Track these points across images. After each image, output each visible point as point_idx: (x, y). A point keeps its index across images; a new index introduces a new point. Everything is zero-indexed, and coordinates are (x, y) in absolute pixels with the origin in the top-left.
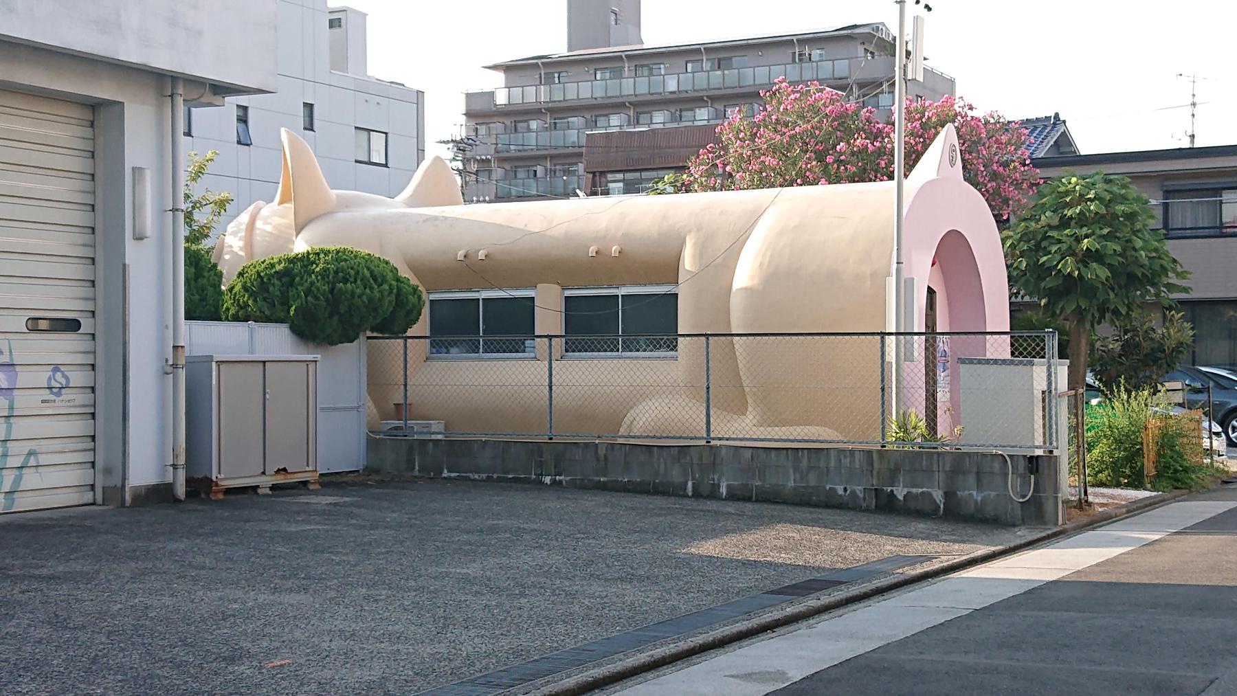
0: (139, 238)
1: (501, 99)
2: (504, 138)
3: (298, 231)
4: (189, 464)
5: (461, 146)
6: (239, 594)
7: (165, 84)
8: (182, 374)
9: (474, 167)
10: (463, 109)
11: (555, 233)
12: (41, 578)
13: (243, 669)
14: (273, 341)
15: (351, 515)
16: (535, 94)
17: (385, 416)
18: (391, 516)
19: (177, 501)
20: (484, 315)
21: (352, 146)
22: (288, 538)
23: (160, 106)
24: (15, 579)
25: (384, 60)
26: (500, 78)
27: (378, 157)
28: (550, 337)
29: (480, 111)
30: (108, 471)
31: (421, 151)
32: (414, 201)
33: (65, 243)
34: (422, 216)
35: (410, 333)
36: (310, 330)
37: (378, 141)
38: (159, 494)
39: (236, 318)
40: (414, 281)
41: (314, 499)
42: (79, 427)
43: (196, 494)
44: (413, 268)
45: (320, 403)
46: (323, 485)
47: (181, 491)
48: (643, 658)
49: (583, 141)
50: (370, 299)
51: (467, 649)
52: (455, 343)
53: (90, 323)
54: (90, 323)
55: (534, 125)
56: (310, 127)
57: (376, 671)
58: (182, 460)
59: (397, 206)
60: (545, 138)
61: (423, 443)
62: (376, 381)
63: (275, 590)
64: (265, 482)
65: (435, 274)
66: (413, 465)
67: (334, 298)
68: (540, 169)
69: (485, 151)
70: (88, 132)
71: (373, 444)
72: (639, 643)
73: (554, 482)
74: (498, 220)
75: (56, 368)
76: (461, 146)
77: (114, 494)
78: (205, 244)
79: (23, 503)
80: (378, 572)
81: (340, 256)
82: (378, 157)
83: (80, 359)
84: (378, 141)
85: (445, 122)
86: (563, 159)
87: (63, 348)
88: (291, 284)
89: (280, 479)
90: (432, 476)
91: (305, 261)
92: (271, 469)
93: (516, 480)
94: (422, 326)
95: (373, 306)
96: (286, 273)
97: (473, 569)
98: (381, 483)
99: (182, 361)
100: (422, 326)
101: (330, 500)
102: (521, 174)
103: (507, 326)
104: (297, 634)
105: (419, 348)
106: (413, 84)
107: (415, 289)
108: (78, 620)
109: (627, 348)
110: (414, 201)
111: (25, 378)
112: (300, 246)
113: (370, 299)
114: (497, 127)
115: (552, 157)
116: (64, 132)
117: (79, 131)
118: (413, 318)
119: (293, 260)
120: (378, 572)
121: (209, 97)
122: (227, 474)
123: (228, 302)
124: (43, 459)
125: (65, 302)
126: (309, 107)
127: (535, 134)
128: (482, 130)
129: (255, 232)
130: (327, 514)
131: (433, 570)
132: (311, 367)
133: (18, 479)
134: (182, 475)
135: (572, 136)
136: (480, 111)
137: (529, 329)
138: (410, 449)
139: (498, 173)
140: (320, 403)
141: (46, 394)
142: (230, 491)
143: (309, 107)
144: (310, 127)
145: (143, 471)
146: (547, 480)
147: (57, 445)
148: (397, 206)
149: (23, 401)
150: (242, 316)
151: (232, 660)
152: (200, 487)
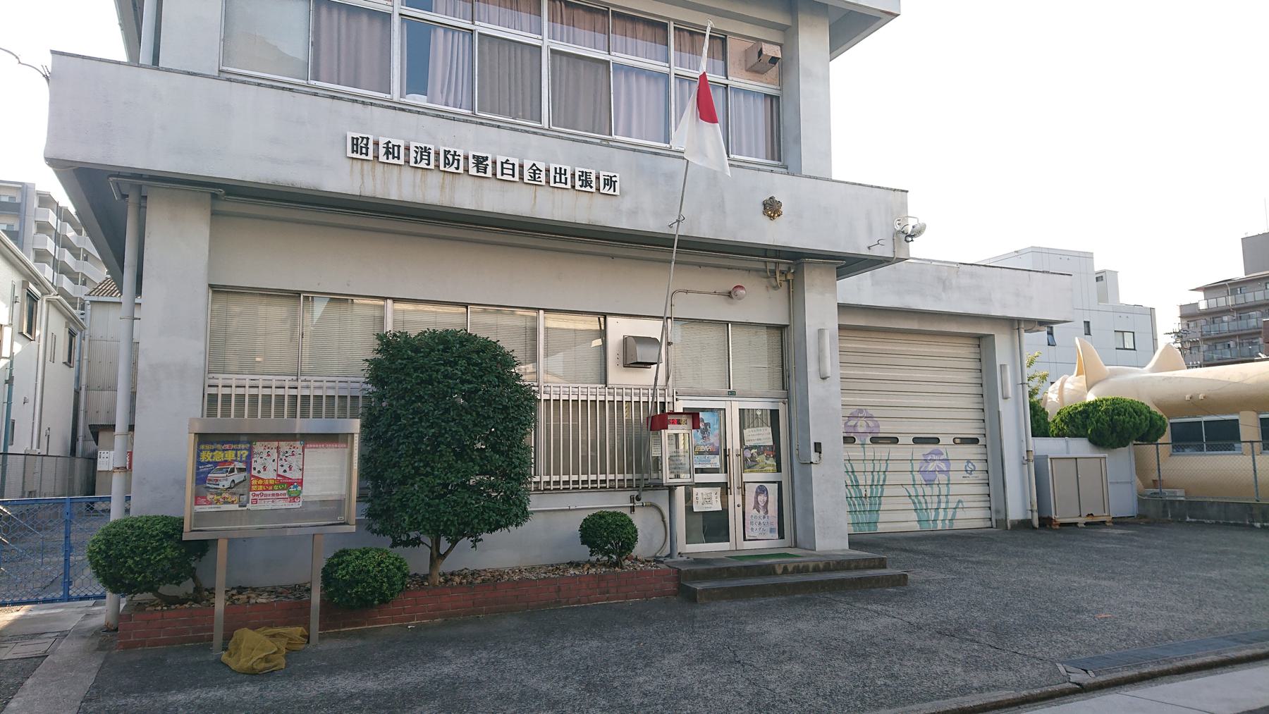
0: (1005, 398)
1: (1203, 306)
2: (1206, 328)
3: (1089, 388)
4: (1039, 511)
5: (1179, 335)
6: (1076, 579)
7: (1015, 324)
8: (1032, 465)
9: (1188, 345)
10: (1178, 314)
11: (1249, 382)
12: (972, 562)
13: (1084, 617)
14: (1079, 447)
15: (1132, 540)
16: (1223, 301)
17: (1146, 487)
18: (1157, 542)
19: (1034, 528)
20: (1208, 429)
21: (1114, 341)
22: (1098, 551)
23: (1012, 334)
24: (961, 562)
25: (1128, 295)
26: (1201, 295)
27: (1129, 345)
28: (1252, 442)
29: (1189, 314)
30: (997, 512)
31: (1155, 340)
32: (1157, 368)
33: (970, 402)
34: (1162, 376)
35: (1159, 441)
36: (1098, 441)
37: (1128, 337)
38: (1025, 525)
39: (1058, 436)
40: (1160, 413)
41: (1110, 531)
42: (981, 489)
43: (1043, 525)
44: (1158, 405)
45: (1114, 480)
46: (1115, 523)
47: (1036, 523)
48: (1247, 652)
49: (1261, 324)
50: (1135, 424)
51: (1217, 619)
52: (1188, 447)
53: (984, 438)
54: (984, 438)
55: (1225, 318)
56: (1088, 333)
57: (1161, 626)
58: (1035, 508)
59: (1145, 373)
60: (1234, 326)
61: (1172, 502)
62: (1141, 470)
63: (1096, 578)
64: (1081, 521)
65: (1174, 408)
66: (1164, 514)
67: (1113, 425)
68: (1232, 344)
69: (1195, 336)
70: (977, 350)
71: (1141, 502)
72: (1251, 641)
73: (1263, 527)
74: (1224, 378)
75: (968, 461)
76: (1179, 335)
77: (1001, 523)
78: (1036, 398)
79: (958, 525)
80: (1154, 572)
81: (1114, 401)
82: (1129, 345)
83: (979, 457)
84: (1128, 337)
85: (1168, 322)
86: (1249, 336)
87: (970, 451)
88: (1088, 417)
89: (1089, 520)
90: (1179, 520)
91: (1094, 405)
92: (1084, 514)
93: (1236, 524)
94: (1166, 437)
95: (1136, 428)
96: (1084, 411)
97: (1214, 574)
98: (1148, 524)
99: (1032, 458)
100: (1166, 437)
101: (1120, 531)
102: (1219, 347)
103: (1223, 436)
104: (1112, 602)
105: (1165, 450)
106: (1147, 305)
107: (1161, 418)
108: (995, 585)
109: (1211, 448)
110: (1157, 368)
111: (954, 466)
112: (1091, 397)
113: (1135, 424)
114: (1202, 322)
115: (1240, 336)
116: (965, 351)
117: (973, 350)
118: (1160, 432)
119: (1089, 404)
120: (1154, 572)
121: (1037, 327)
122: (1060, 516)
123: (1052, 427)
124: (965, 505)
125: (970, 430)
126: (1087, 324)
127: (1227, 324)
128: (1192, 324)
129: (1066, 390)
130: (1119, 539)
131: (1187, 573)
132: (716, 461)
133: (954, 514)
134: (1036, 515)
135: (1253, 322)
136: (1189, 314)
137: (1236, 437)
138: (1165, 506)
139: (1204, 347)
140: (1114, 480)
141: (965, 474)
142: (1062, 525)
143: (1087, 324)
144: (1088, 333)
145: (1016, 512)
146: (1258, 525)
147: (971, 498)
148: (1145, 373)
149: (955, 477)
150: (1061, 434)
151: (1078, 612)
152: (1046, 522)
